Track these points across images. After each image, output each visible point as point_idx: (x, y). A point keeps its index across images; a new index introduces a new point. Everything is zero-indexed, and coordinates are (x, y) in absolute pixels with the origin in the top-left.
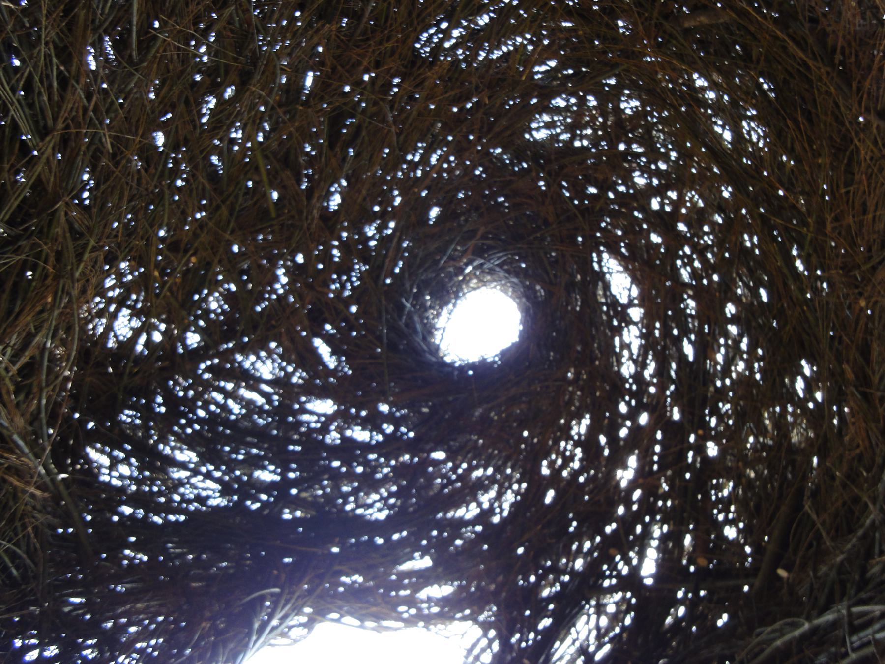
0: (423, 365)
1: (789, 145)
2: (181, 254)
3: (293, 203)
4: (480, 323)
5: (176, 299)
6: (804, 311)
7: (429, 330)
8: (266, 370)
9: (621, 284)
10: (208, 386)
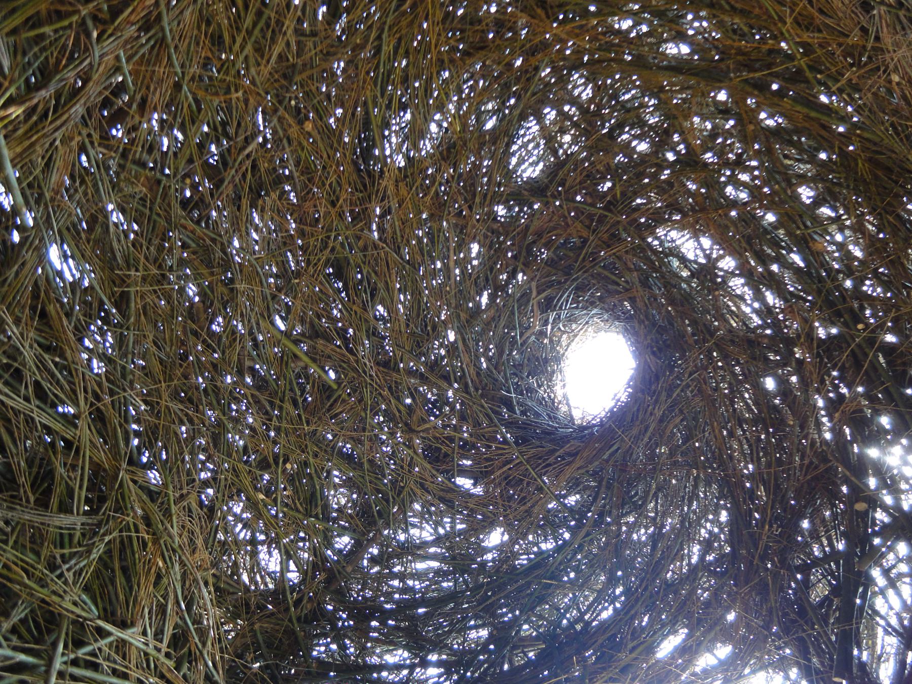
0: (565, 440)
1: (727, 7)
2: (273, 469)
3: (345, 365)
4: (594, 370)
5: (298, 511)
6: (859, 136)
7: (551, 406)
8: (426, 533)
9: (692, 247)
10: (380, 578)
